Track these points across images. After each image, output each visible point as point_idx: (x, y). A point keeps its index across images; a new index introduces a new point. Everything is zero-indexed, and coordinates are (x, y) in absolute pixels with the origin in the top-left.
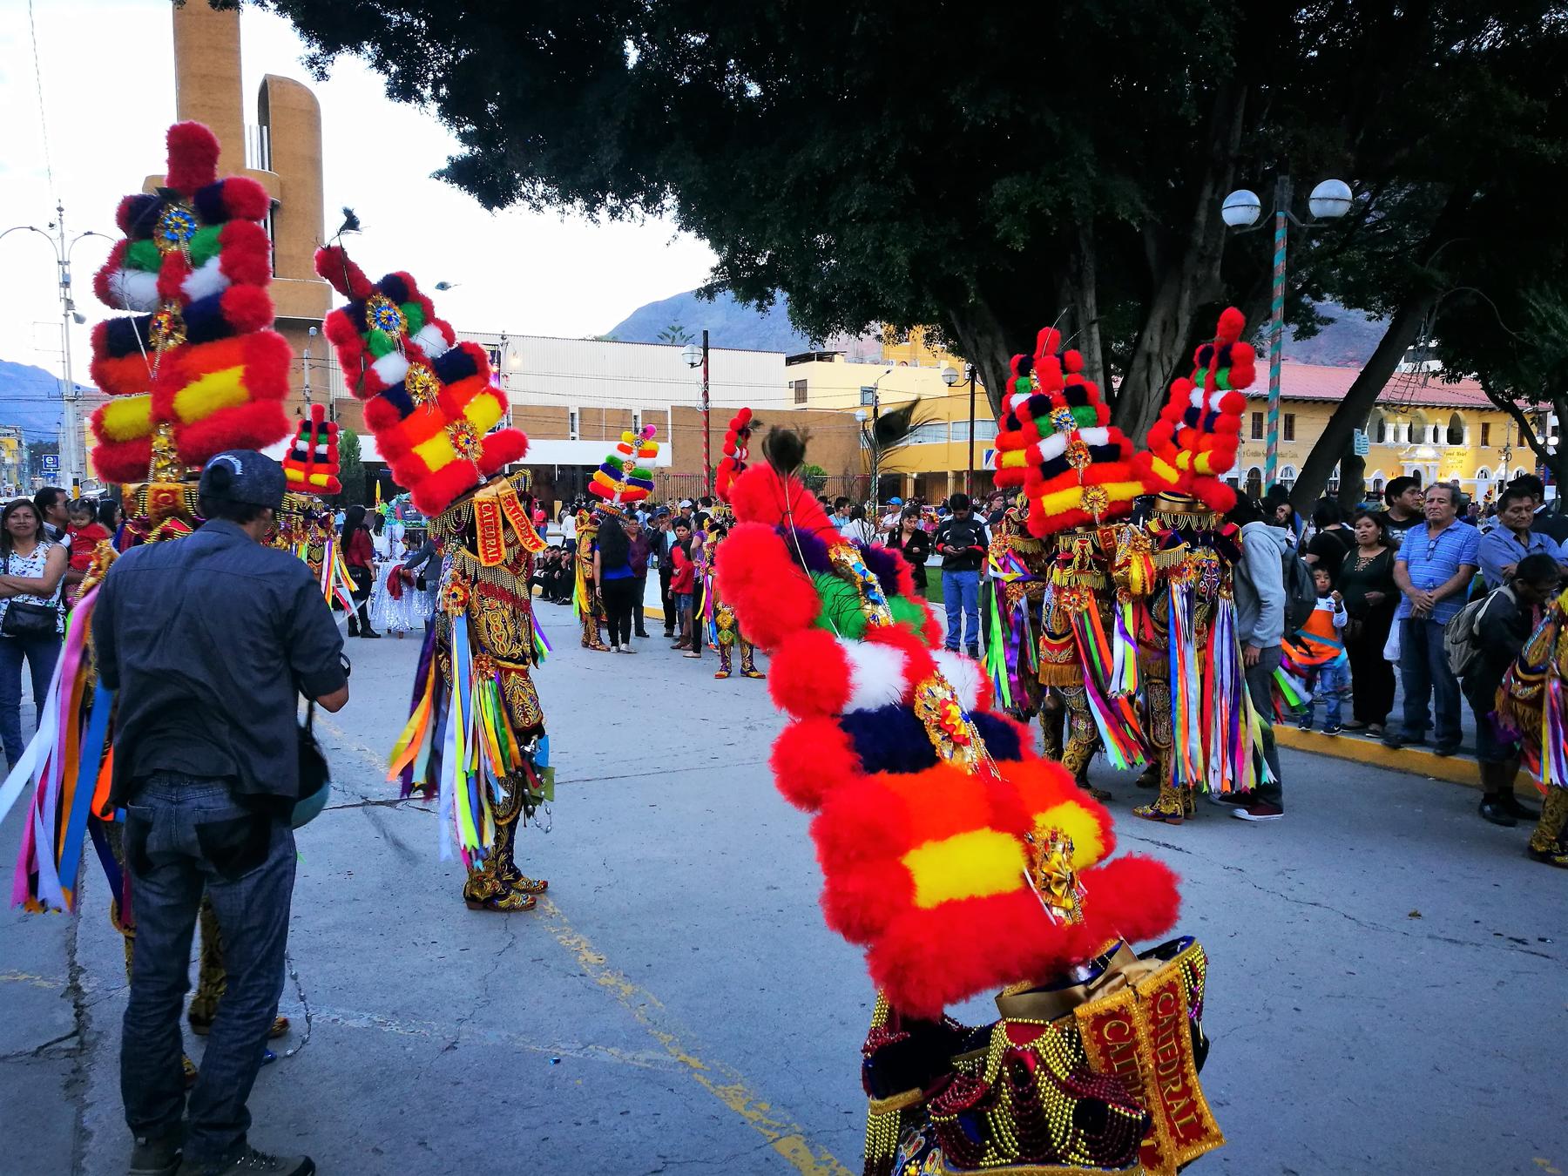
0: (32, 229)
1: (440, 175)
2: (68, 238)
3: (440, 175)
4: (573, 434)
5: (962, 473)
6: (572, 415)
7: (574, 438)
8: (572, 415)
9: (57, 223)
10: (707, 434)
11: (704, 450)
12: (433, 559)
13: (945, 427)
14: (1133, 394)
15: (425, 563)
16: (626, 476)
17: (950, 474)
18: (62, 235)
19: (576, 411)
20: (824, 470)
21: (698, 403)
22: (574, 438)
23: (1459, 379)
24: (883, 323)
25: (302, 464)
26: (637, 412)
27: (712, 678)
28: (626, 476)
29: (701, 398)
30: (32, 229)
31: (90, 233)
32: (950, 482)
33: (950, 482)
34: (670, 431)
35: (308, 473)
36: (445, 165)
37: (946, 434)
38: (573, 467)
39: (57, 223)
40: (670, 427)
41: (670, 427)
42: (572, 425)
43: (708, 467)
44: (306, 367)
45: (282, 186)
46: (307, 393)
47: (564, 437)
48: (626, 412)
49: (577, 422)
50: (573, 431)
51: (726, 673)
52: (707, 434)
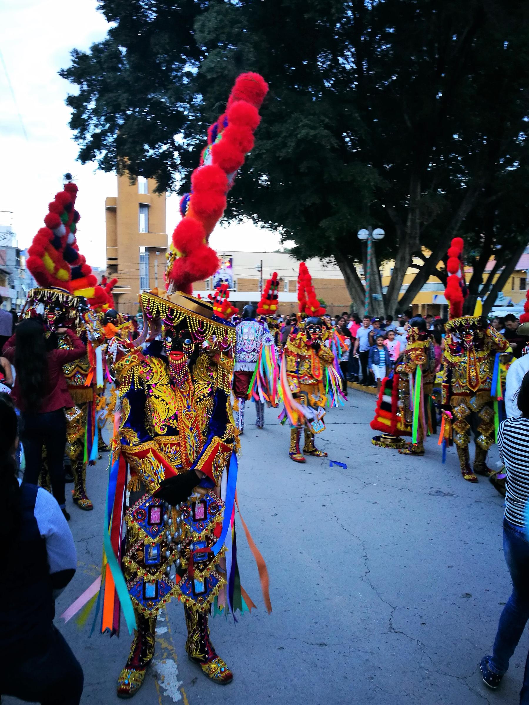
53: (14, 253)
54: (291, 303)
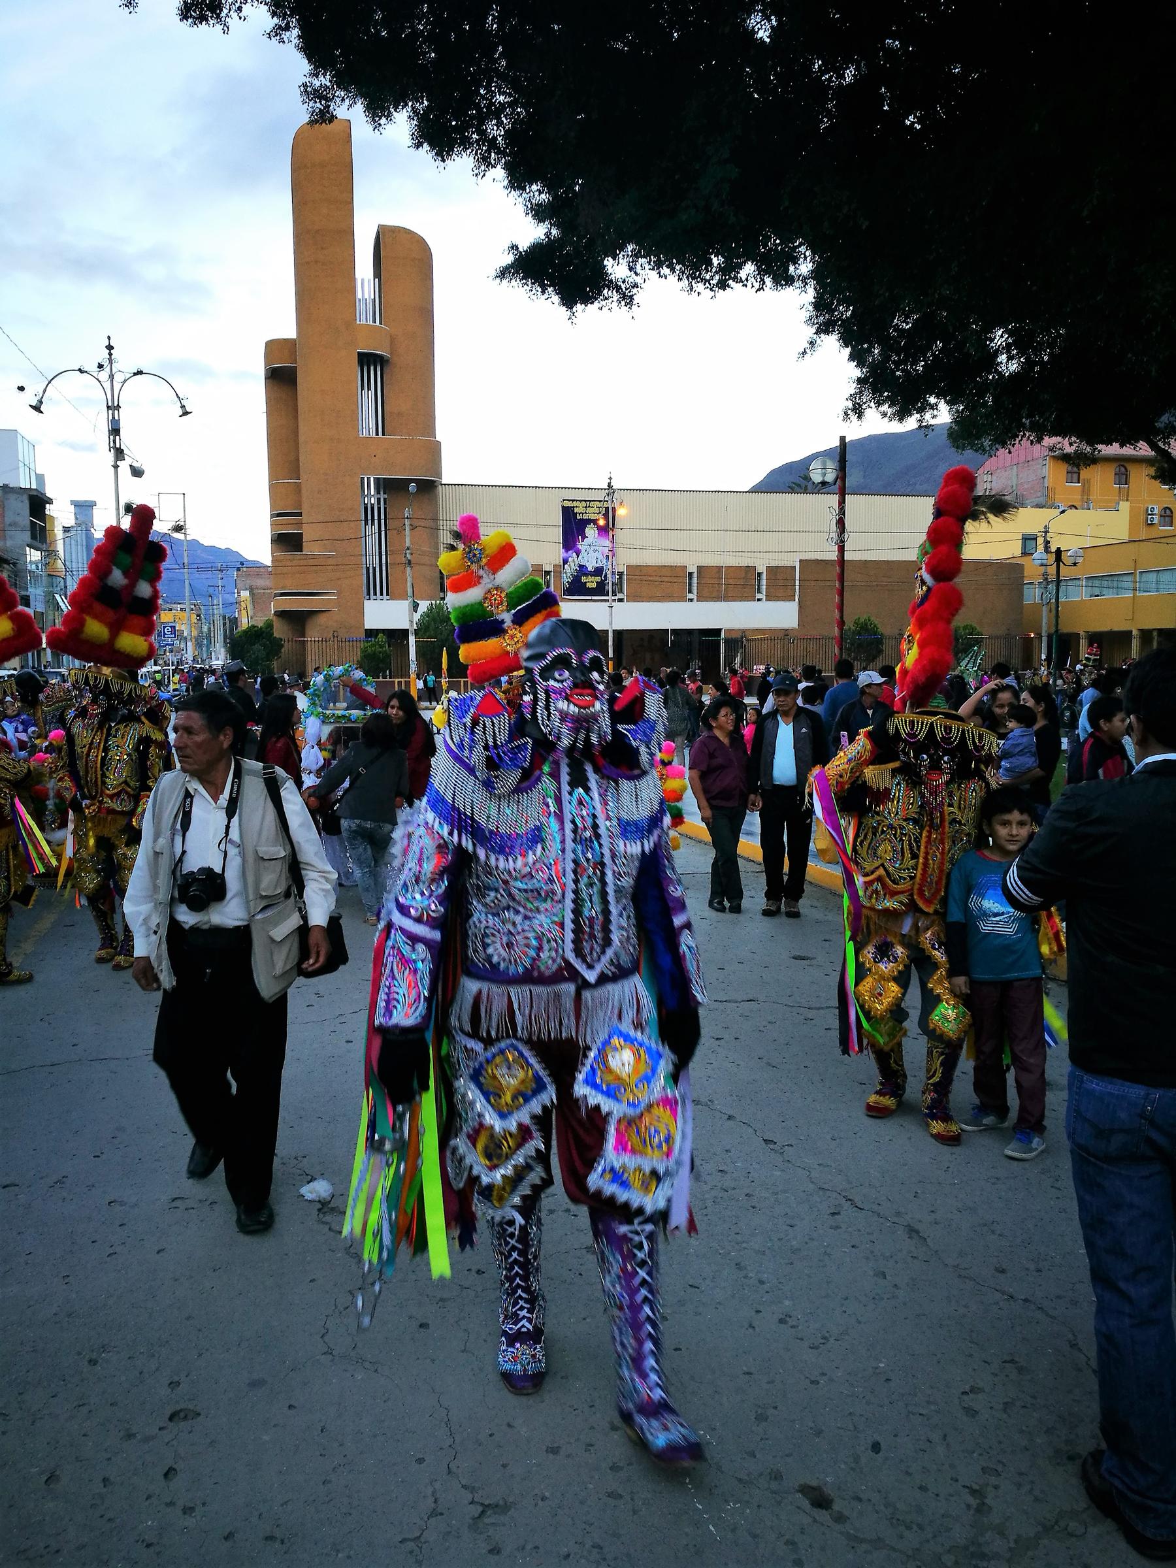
0: (81, 371)
1: (504, 273)
2: (118, 378)
3: (504, 273)
4: (690, 596)
5: (1150, 632)
6: (691, 574)
7: (691, 600)
8: (691, 574)
9: (106, 364)
10: (841, 593)
11: (837, 614)
12: (358, 783)
13: (1129, 578)
14: (162, 794)
15: (346, 784)
16: (507, 617)
17: (1135, 633)
18: (112, 377)
19: (695, 570)
20: (978, 629)
21: (834, 556)
22: (691, 600)
23: (965, 628)
24: (1073, 439)
25: (111, 615)
26: (761, 568)
27: (861, 1112)
28: (507, 617)
29: (834, 528)
30: (81, 371)
31: (140, 373)
32: (1135, 644)
33: (1135, 644)
34: (797, 588)
35: (116, 629)
36: (509, 259)
37: (1131, 585)
38: (690, 632)
39: (106, 364)
40: (797, 583)
41: (797, 583)
42: (690, 584)
43: (841, 623)
44: (407, 528)
45: (393, 340)
46: (408, 556)
47: (682, 598)
48: (750, 569)
49: (695, 580)
50: (690, 592)
51: (888, 1101)
52: (841, 593)
53: (24, 507)
54: (744, 631)
